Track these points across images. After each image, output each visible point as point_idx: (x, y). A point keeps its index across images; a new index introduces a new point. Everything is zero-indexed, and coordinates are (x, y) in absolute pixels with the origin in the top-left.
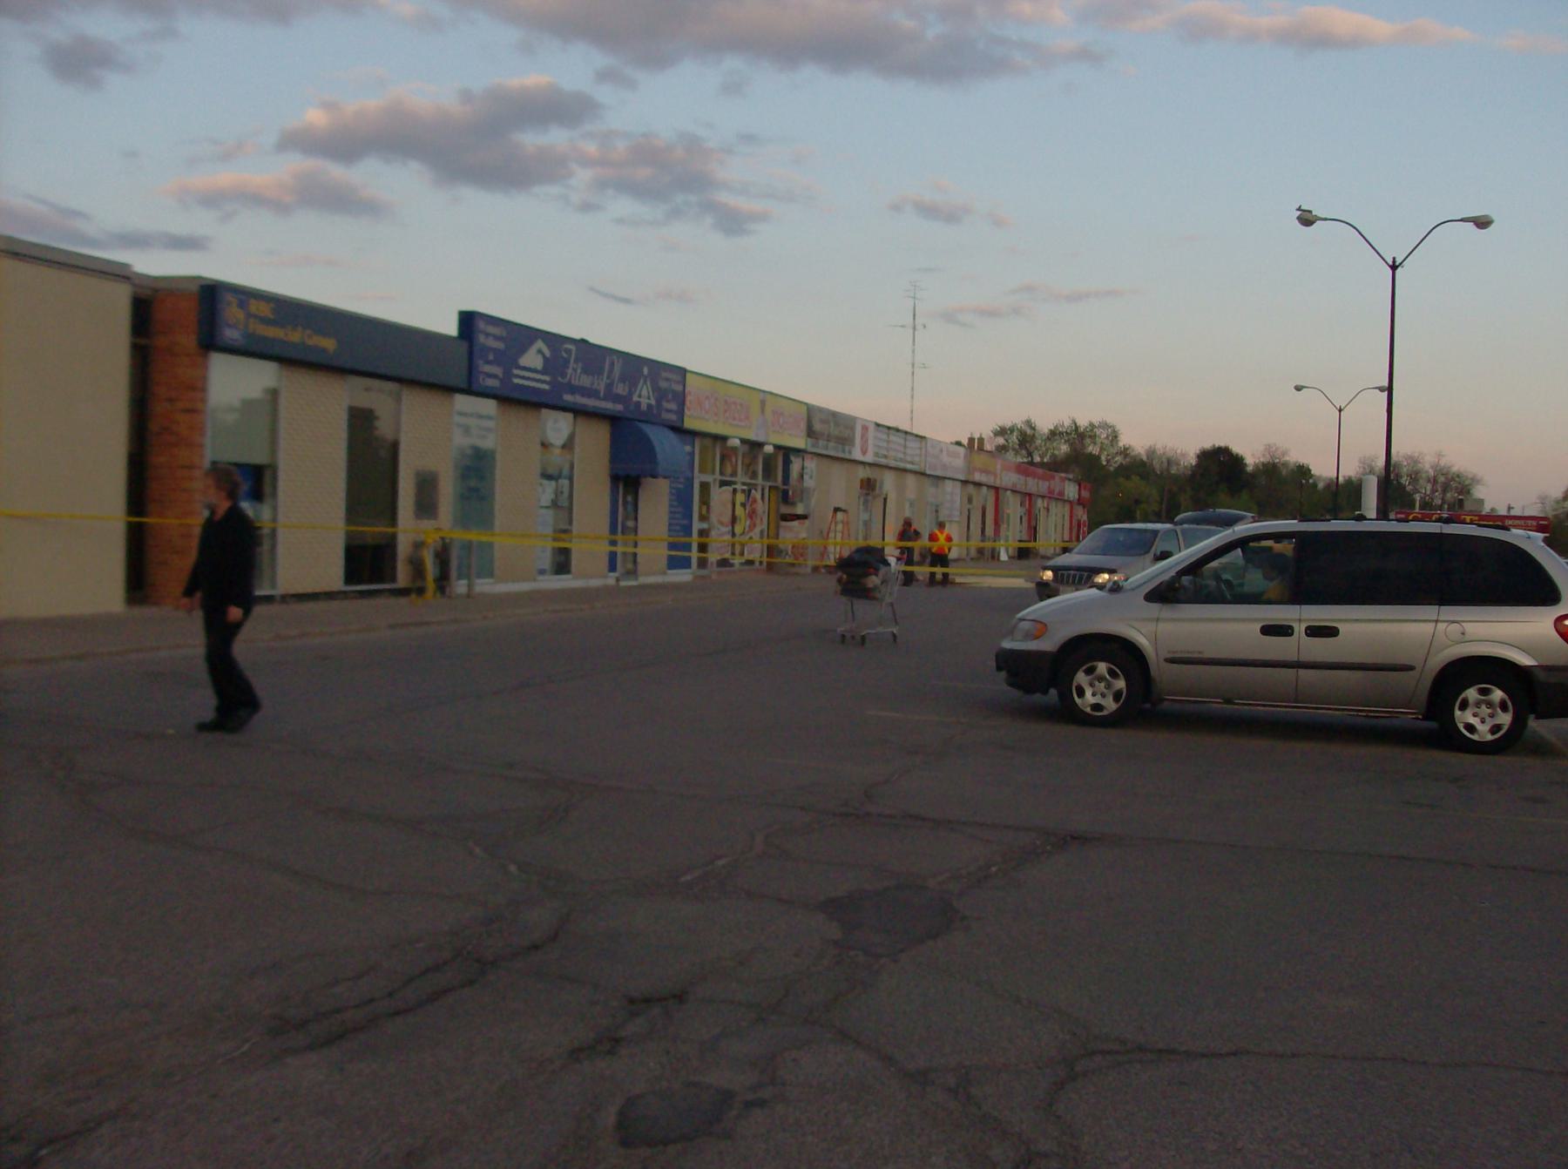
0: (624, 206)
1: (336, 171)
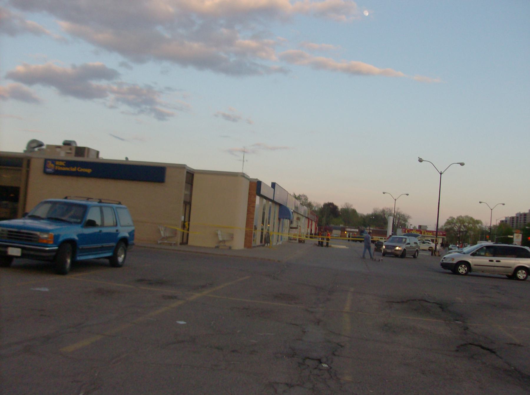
0: (125, 108)
1: (25, 88)
